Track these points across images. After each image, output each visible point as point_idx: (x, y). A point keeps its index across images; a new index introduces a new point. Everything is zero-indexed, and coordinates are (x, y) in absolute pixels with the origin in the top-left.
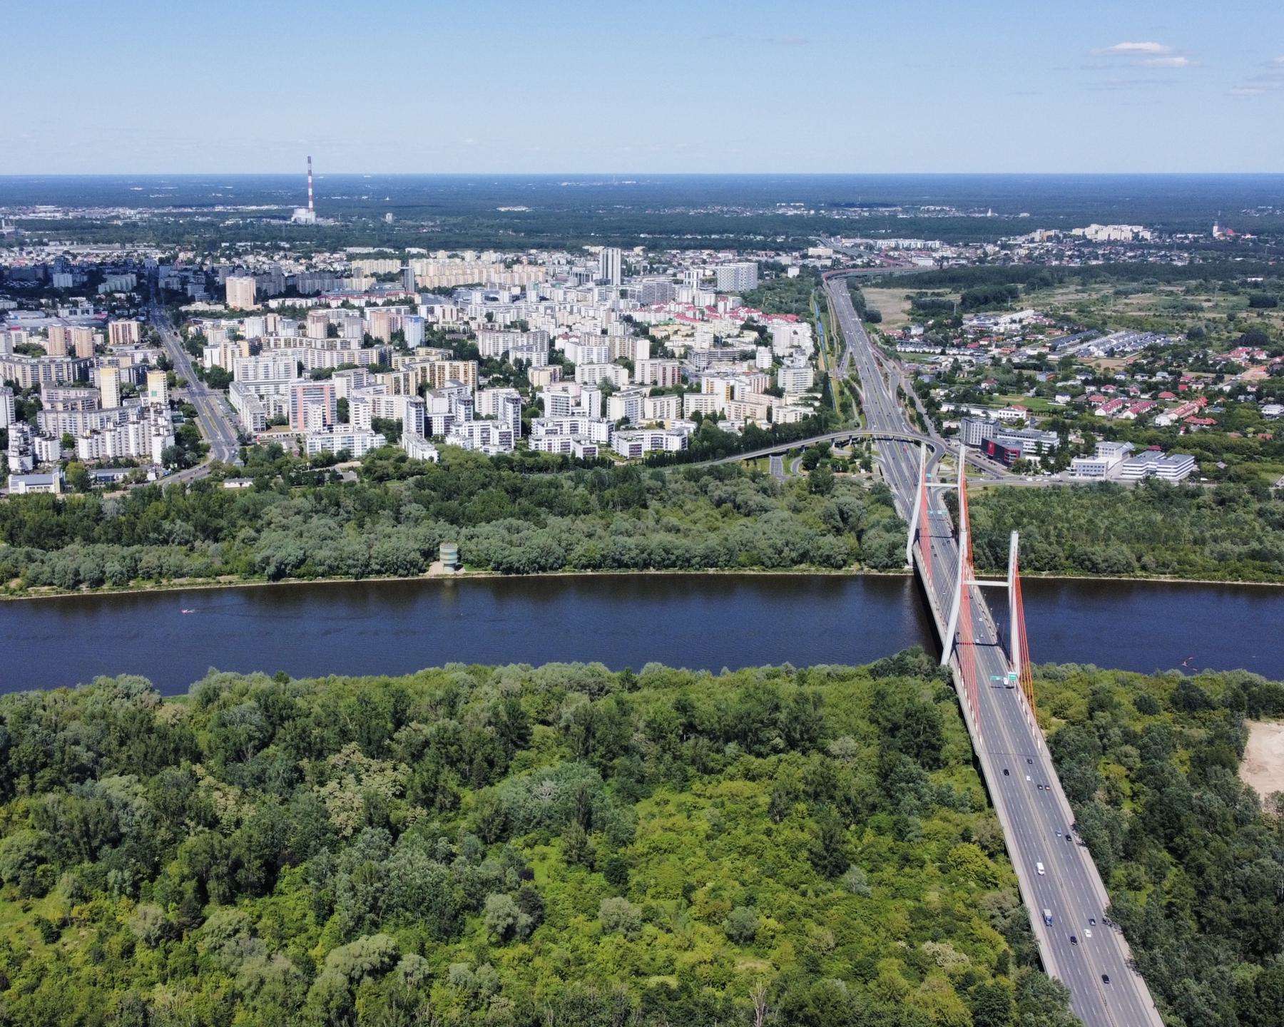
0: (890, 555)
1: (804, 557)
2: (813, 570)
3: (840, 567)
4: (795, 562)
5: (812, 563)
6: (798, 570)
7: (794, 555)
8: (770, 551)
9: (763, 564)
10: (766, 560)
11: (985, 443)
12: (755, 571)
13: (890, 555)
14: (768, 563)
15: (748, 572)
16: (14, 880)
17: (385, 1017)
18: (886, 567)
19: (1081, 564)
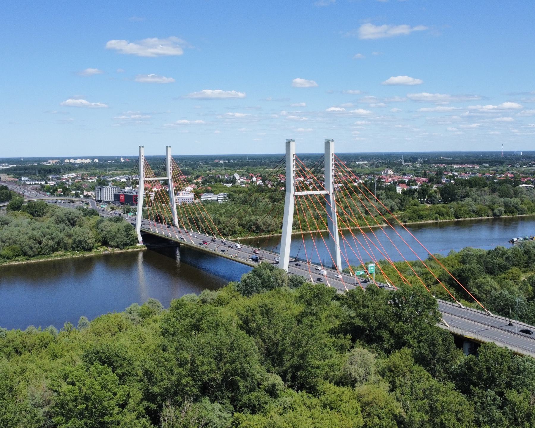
0: (128, 235)
1: (59, 246)
2: (69, 255)
3: (90, 250)
4: (54, 250)
5: (66, 249)
6: (56, 257)
7: (51, 243)
8: (31, 242)
9: (25, 254)
10: (28, 250)
11: (117, 196)
12: (21, 261)
13: (128, 235)
14: (31, 253)
15: (13, 263)
16: (522, 426)
17: (90, 423)
18: (126, 245)
19: (249, 228)
